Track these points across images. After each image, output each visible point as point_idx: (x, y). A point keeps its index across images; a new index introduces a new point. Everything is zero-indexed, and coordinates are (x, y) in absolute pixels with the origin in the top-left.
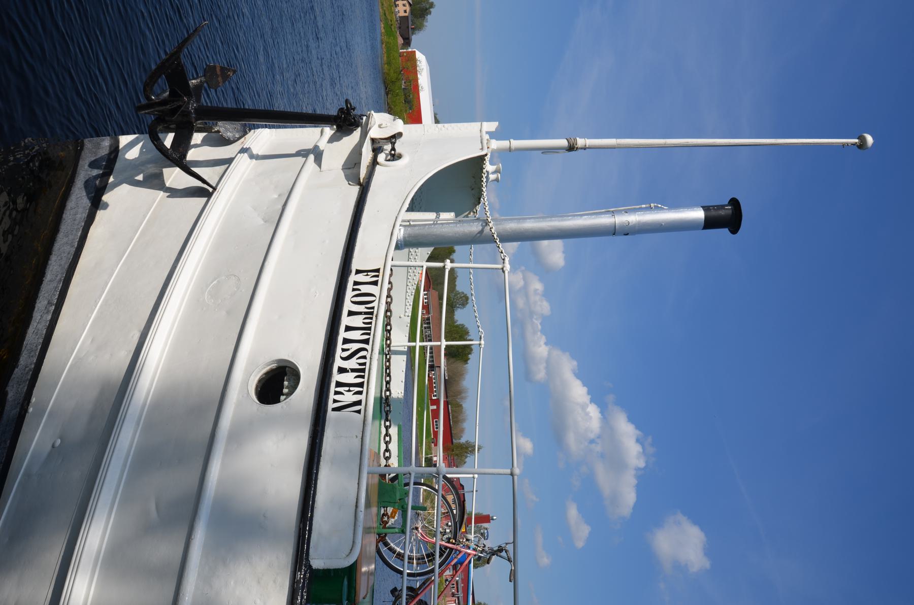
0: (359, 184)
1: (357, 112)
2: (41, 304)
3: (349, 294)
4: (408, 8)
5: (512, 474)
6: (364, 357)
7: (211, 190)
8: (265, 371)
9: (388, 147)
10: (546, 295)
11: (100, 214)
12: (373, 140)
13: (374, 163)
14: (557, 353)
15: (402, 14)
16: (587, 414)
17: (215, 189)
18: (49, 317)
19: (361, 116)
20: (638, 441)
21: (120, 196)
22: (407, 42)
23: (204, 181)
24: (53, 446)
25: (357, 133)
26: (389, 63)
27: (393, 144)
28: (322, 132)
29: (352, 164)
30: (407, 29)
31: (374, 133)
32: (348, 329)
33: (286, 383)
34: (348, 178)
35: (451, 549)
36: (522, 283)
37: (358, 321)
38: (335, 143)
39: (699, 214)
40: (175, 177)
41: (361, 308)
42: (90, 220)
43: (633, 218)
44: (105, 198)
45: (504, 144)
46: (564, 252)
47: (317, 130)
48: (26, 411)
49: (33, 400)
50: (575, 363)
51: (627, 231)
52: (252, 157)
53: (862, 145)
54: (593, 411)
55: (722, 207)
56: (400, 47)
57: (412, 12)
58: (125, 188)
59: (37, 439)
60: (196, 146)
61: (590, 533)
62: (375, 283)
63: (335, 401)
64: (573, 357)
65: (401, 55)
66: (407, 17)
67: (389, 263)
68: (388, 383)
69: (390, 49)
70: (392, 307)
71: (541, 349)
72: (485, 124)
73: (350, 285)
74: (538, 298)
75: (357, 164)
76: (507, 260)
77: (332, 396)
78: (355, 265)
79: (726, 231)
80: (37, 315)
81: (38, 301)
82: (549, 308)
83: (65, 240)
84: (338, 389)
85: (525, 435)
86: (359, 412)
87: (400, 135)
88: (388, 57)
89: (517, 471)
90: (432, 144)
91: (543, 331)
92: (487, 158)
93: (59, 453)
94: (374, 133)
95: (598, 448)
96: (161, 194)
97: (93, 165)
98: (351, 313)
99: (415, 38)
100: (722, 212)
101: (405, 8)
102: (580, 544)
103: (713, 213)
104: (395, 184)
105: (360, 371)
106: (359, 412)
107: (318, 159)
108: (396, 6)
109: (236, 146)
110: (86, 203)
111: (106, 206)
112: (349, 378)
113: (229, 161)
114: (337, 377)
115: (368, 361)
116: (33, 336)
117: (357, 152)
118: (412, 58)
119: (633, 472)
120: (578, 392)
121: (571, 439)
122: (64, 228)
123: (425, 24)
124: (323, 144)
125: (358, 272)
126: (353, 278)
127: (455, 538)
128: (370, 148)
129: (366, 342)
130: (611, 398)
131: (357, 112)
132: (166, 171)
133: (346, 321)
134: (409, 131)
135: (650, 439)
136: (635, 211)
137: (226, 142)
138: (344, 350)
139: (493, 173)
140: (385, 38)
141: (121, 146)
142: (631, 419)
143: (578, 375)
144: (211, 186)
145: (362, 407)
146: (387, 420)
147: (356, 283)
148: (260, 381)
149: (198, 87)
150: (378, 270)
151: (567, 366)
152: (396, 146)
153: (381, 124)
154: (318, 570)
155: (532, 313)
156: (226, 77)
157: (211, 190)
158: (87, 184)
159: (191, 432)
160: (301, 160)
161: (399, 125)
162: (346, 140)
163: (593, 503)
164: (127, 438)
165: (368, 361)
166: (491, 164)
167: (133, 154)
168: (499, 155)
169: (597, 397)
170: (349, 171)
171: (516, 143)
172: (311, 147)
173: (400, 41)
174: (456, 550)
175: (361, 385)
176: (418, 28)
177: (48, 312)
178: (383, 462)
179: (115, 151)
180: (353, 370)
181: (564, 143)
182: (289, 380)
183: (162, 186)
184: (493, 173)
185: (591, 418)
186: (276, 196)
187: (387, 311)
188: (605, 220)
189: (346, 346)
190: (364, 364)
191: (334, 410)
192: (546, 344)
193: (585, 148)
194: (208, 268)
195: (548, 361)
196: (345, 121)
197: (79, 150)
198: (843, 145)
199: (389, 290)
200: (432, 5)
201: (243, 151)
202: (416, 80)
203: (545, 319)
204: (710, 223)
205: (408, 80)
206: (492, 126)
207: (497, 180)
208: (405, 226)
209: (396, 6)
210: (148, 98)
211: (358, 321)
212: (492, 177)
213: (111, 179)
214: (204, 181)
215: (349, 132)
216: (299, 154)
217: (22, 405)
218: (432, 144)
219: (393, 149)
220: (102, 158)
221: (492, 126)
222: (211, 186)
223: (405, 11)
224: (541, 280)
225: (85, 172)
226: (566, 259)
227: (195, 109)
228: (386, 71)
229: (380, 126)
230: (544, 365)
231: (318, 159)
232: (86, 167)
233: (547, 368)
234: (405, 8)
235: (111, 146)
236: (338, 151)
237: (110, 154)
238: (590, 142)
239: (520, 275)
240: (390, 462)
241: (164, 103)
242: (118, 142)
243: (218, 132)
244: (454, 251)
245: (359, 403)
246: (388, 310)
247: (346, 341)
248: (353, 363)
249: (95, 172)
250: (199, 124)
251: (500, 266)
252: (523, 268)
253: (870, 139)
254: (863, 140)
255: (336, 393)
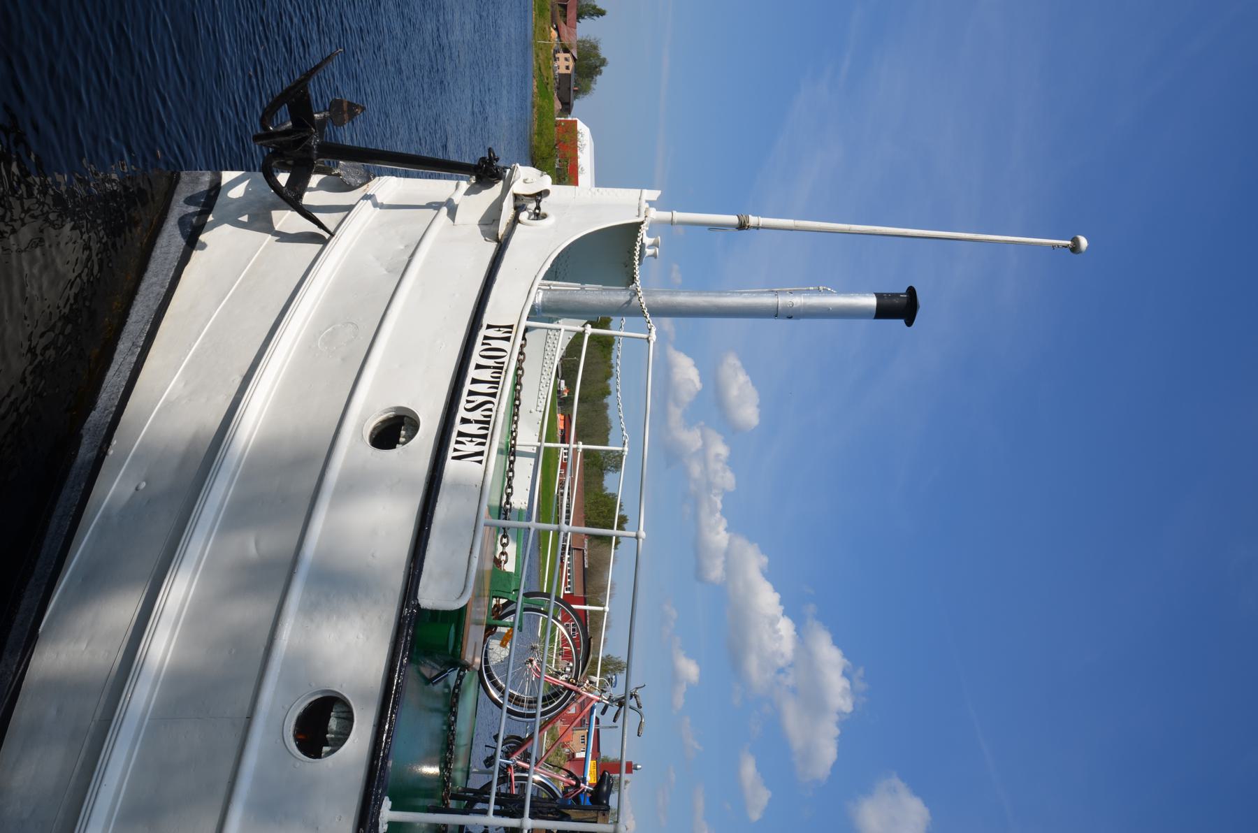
0: (497, 240)
1: (501, 164)
2: (123, 346)
3: (478, 347)
4: (571, 64)
5: (637, 537)
6: (490, 410)
7: (327, 236)
8: (384, 416)
9: (532, 206)
10: (731, 463)
11: (196, 255)
12: (516, 196)
13: (516, 220)
14: (740, 542)
15: (563, 71)
16: (776, 632)
17: (332, 235)
18: (134, 359)
19: (504, 169)
20: (845, 674)
21: (221, 240)
22: (567, 108)
23: (321, 225)
24: (137, 489)
25: (498, 188)
26: (540, 134)
27: (538, 202)
28: (457, 186)
29: (490, 220)
30: (568, 91)
31: (518, 188)
32: (474, 381)
33: (403, 433)
34: (484, 234)
35: (571, 690)
36: (699, 444)
37: (486, 375)
38: (473, 196)
39: (872, 301)
40: (287, 220)
41: (491, 362)
42: (184, 260)
43: (798, 301)
44: (202, 238)
45: (666, 215)
46: (758, 406)
47: (453, 183)
48: (106, 453)
49: (114, 442)
50: (765, 559)
51: (791, 314)
52: (376, 205)
53: (1075, 248)
54: (785, 627)
55: (897, 295)
56: (556, 113)
57: (576, 69)
58: (226, 229)
59: (115, 488)
60: (312, 190)
61: (770, 800)
62: (508, 339)
63: (455, 450)
64: (764, 551)
65: (558, 124)
66: (569, 75)
67: (524, 323)
68: (510, 479)
69: (543, 115)
70: (523, 380)
71: (719, 536)
72: (645, 191)
73: (480, 339)
74: (719, 466)
75: (496, 221)
76: (654, 330)
77: (452, 445)
78: (487, 319)
79: (901, 322)
80: (118, 357)
81: (120, 343)
82: (734, 482)
83: (154, 279)
84: (460, 439)
85: (689, 656)
86: (480, 462)
87: (546, 193)
88: (540, 125)
89: (643, 534)
90: (584, 206)
91: (723, 513)
92: (644, 229)
93: (138, 509)
94: (518, 188)
95: (790, 681)
96: (269, 238)
97: (190, 201)
98: (478, 367)
99: (577, 104)
100: (896, 301)
101: (567, 63)
102: (755, 816)
103: (886, 301)
104: (535, 246)
105: (485, 423)
106: (480, 462)
107: (452, 212)
108: (556, 59)
109: (358, 193)
110: (180, 242)
111: (204, 246)
112: (472, 429)
113: (349, 208)
114: (458, 427)
115: (493, 414)
116: (114, 378)
117: (497, 207)
118: (571, 129)
119: (835, 718)
120: (767, 599)
121: (753, 664)
122: (153, 266)
123: (593, 86)
124: (458, 198)
125: (489, 327)
126: (484, 332)
127: (576, 678)
128: (512, 205)
129: (494, 395)
130: (811, 609)
131: (501, 164)
132: (276, 214)
133: (472, 373)
134: (560, 194)
135: (861, 671)
136: (799, 292)
137: (349, 188)
138: (468, 402)
139: (650, 247)
140: (538, 100)
141: (223, 183)
142: (837, 642)
143: (768, 575)
144: (328, 231)
145: (484, 458)
146: (504, 536)
147: (486, 338)
148: (375, 429)
149: (323, 122)
150: (511, 327)
151: (753, 562)
152: (542, 205)
153: (527, 179)
154: (426, 610)
155: (710, 486)
156: (352, 115)
157: (327, 236)
158: (182, 222)
159: (295, 482)
160: (432, 212)
161: (546, 182)
162: (485, 193)
163: (778, 757)
164: (220, 492)
165: (493, 414)
166: (649, 235)
167: (237, 192)
168: (656, 226)
169: (792, 609)
170: (485, 228)
171: (679, 216)
172: (444, 200)
173: (558, 105)
174: (577, 692)
175: (485, 436)
176: (583, 91)
177: (133, 354)
178: (500, 549)
179: (216, 188)
180: (477, 422)
181: (734, 219)
182: (406, 430)
183: (268, 228)
184: (650, 247)
185: (781, 638)
186: (402, 247)
187: (518, 369)
188: (767, 300)
189: (471, 398)
190: (490, 416)
191: (454, 458)
192: (727, 530)
193: (757, 228)
194: (312, 332)
195: (727, 554)
196: (486, 172)
197: (173, 183)
198: (1053, 246)
199: (522, 346)
200: (603, 62)
201: (366, 197)
202: (575, 158)
203: (727, 496)
204: (885, 310)
205: (563, 157)
206: (654, 195)
207: (654, 256)
208: (541, 594)
209: (556, 59)
210: (265, 128)
211: (486, 375)
212: (649, 252)
213: (211, 218)
214: (321, 225)
215: (489, 185)
216: (429, 206)
217: (101, 448)
218: (584, 206)
219: (538, 208)
220: (201, 194)
221: (654, 195)
222: (328, 231)
223: (567, 68)
224: (726, 442)
225: (179, 208)
226: (760, 416)
227: (318, 145)
228: (535, 143)
229: (525, 181)
230: (723, 558)
231: (452, 212)
232: (181, 203)
233: (726, 562)
234: (567, 63)
235: (211, 182)
236: (473, 205)
237: (209, 191)
238: (763, 221)
239: (697, 433)
240: (507, 549)
241: (287, 133)
242: (220, 177)
243: (339, 175)
244: (609, 393)
245: (481, 453)
246: (519, 368)
247: (471, 393)
248: (477, 415)
249: (192, 209)
250: (320, 162)
251: (645, 336)
252: (702, 423)
253: (1084, 242)
254: (1075, 241)
255: (457, 442)
